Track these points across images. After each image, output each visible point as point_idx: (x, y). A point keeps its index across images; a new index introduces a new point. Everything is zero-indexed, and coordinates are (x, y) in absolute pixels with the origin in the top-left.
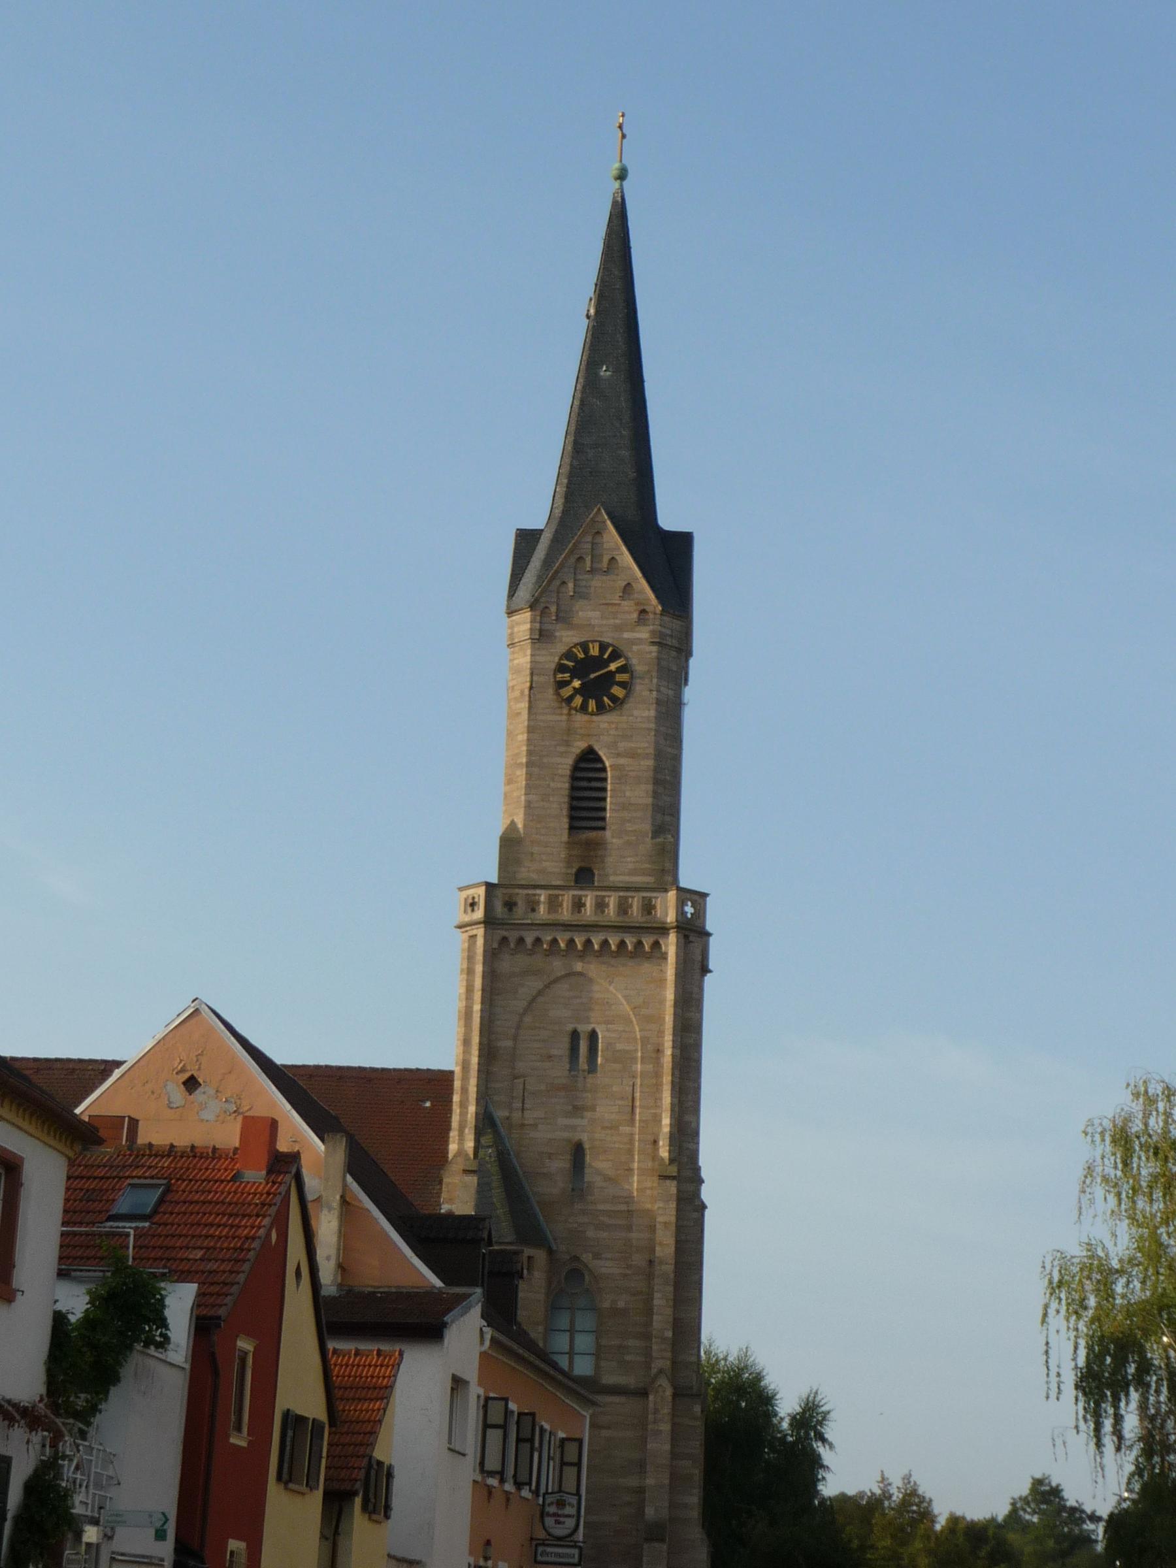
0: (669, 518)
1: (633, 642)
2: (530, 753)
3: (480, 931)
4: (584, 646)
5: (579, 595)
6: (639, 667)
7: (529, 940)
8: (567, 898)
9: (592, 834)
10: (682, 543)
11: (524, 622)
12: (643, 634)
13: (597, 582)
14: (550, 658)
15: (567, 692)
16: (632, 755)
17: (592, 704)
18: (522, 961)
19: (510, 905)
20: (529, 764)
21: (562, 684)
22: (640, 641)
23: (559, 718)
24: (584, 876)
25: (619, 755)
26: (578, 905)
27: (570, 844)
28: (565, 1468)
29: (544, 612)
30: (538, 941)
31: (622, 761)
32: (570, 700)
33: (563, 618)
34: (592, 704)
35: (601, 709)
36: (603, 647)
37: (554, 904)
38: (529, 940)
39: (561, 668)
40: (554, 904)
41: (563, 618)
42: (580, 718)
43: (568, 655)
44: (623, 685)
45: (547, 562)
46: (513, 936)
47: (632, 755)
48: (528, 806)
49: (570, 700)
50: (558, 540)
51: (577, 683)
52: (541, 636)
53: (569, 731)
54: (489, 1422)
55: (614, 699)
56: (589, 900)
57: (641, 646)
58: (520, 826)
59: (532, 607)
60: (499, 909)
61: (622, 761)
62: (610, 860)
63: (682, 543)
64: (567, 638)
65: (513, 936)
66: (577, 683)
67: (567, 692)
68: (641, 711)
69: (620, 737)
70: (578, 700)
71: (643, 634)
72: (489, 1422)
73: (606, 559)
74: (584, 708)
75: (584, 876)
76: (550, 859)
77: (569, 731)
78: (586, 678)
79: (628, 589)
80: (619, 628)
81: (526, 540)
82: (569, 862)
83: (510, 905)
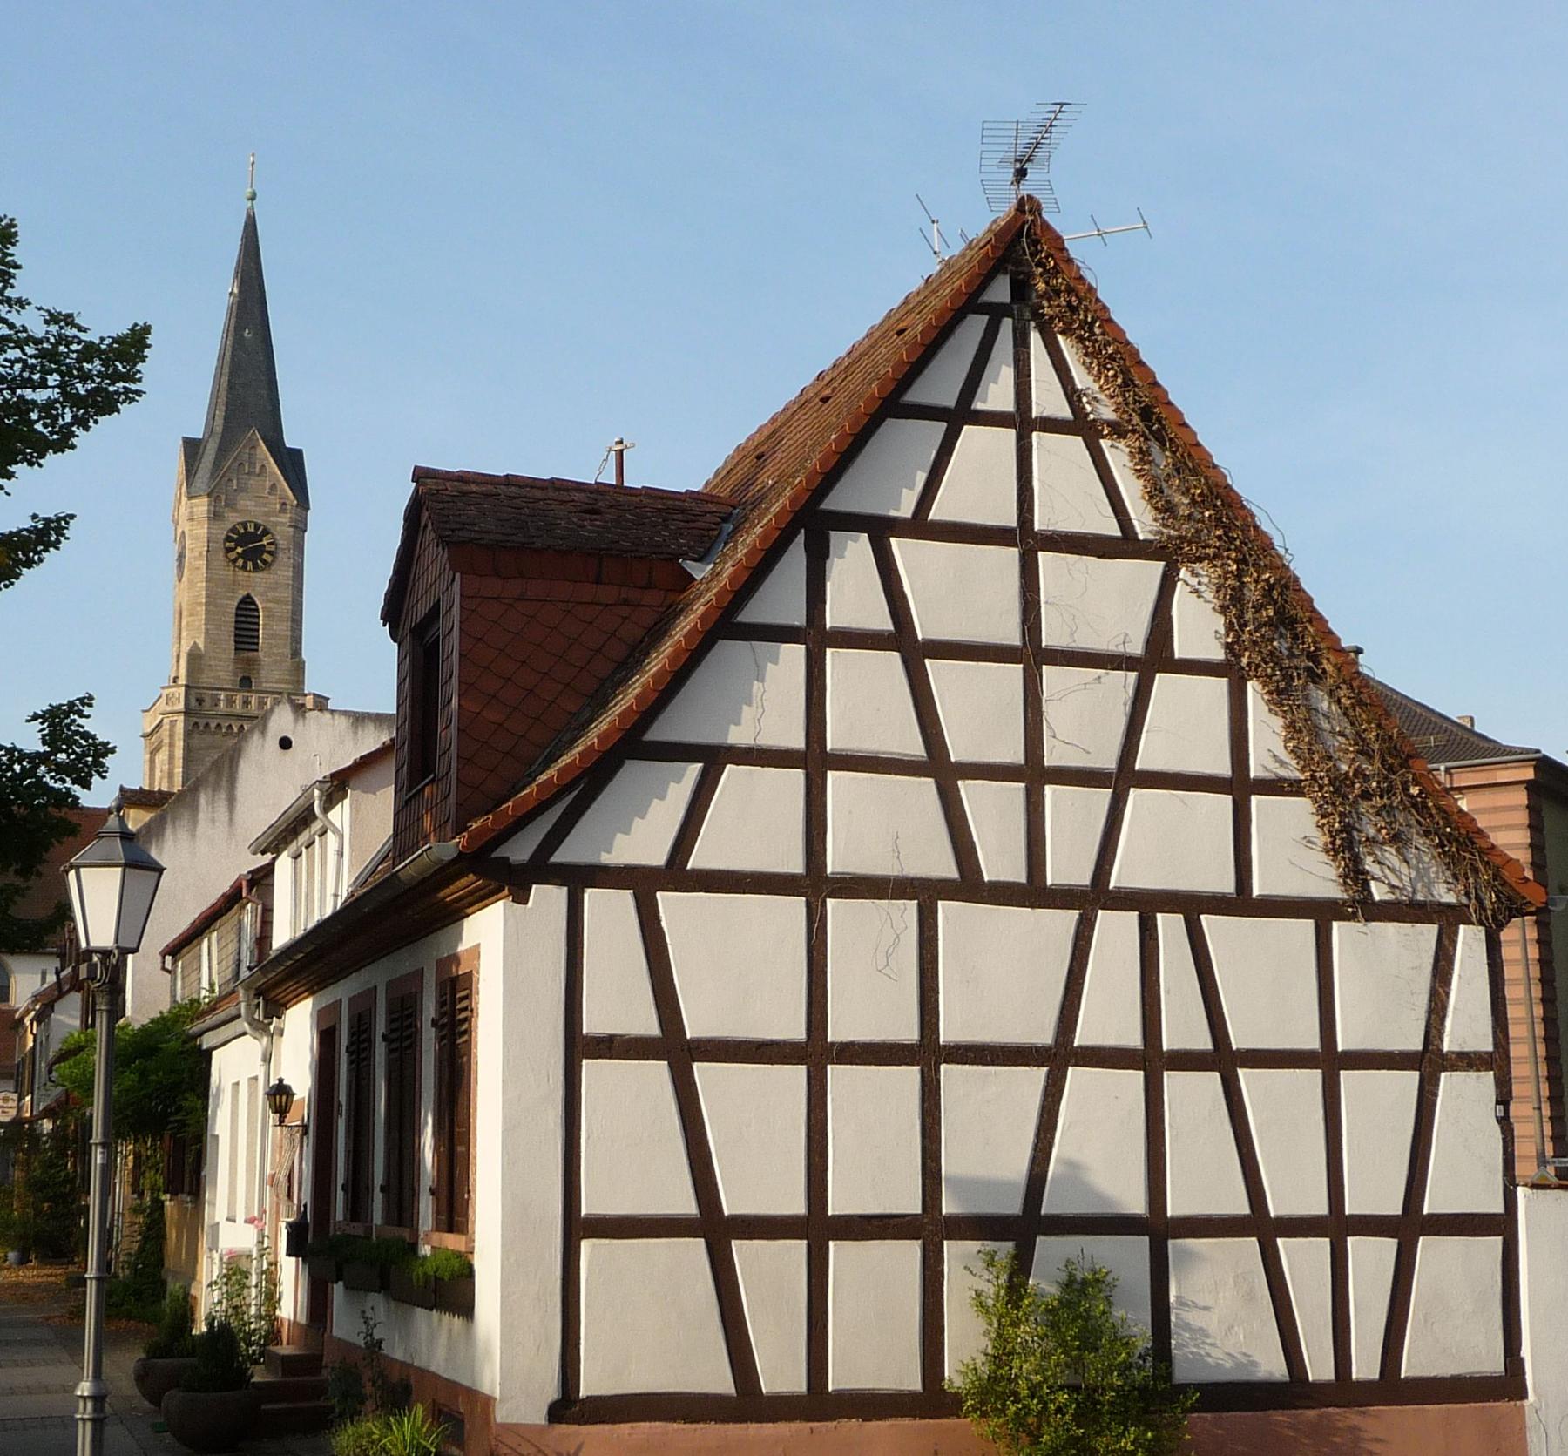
0: (290, 442)
1: (277, 524)
2: (207, 596)
3: (181, 718)
4: (244, 525)
5: (240, 490)
6: (282, 543)
7: (213, 725)
8: (239, 698)
9: (250, 654)
10: (298, 454)
11: (202, 506)
12: (285, 518)
13: (253, 481)
14: (222, 531)
15: (232, 555)
16: (277, 601)
17: (250, 564)
18: (208, 739)
19: (200, 701)
20: (207, 604)
21: (229, 550)
22: (283, 524)
23: (228, 573)
24: (245, 683)
25: (268, 601)
26: (246, 703)
27: (236, 661)
28: (589, 1068)
29: (217, 499)
30: (219, 725)
31: (270, 605)
32: (235, 561)
33: (230, 504)
34: (250, 564)
35: (256, 568)
36: (257, 526)
37: (230, 702)
38: (213, 725)
39: (228, 539)
40: (230, 702)
41: (230, 504)
42: (241, 573)
43: (234, 530)
44: (270, 553)
45: (217, 465)
46: (202, 722)
47: (277, 601)
48: (207, 632)
49: (235, 561)
50: (222, 451)
51: (240, 550)
52: (215, 516)
53: (234, 582)
54: (591, 1024)
55: (265, 562)
56: (239, 698)
57: (281, 525)
58: (201, 646)
59: (209, 496)
60: (193, 703)
61: (270, 605)
62: (263, 672)
63: (298, 454)
64: (233, 519)
65: (202, 722)
66: (240, 550)
67: (232, 555)
68: (282, 572)
69: (258, 584)
70: (241, 561)
71: (285, 518)
72: (591, 1024)
73: (258, 466)
74: (244, 568)
75: (245, 683)
76: (222, 671)
77: (234, 582)
78: (248, 547)
79: (273, 487)
80: (267, 514)
81: (192, 448)
82: (235, 674)
83: (200, 701)
